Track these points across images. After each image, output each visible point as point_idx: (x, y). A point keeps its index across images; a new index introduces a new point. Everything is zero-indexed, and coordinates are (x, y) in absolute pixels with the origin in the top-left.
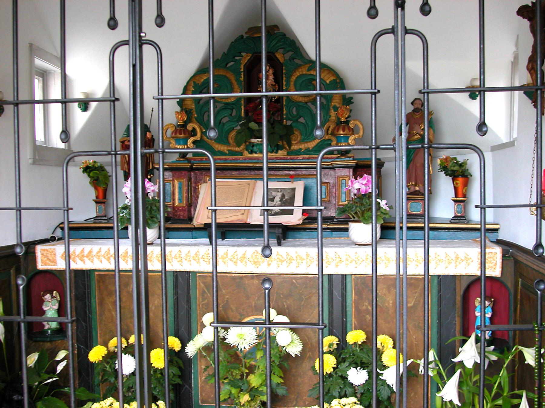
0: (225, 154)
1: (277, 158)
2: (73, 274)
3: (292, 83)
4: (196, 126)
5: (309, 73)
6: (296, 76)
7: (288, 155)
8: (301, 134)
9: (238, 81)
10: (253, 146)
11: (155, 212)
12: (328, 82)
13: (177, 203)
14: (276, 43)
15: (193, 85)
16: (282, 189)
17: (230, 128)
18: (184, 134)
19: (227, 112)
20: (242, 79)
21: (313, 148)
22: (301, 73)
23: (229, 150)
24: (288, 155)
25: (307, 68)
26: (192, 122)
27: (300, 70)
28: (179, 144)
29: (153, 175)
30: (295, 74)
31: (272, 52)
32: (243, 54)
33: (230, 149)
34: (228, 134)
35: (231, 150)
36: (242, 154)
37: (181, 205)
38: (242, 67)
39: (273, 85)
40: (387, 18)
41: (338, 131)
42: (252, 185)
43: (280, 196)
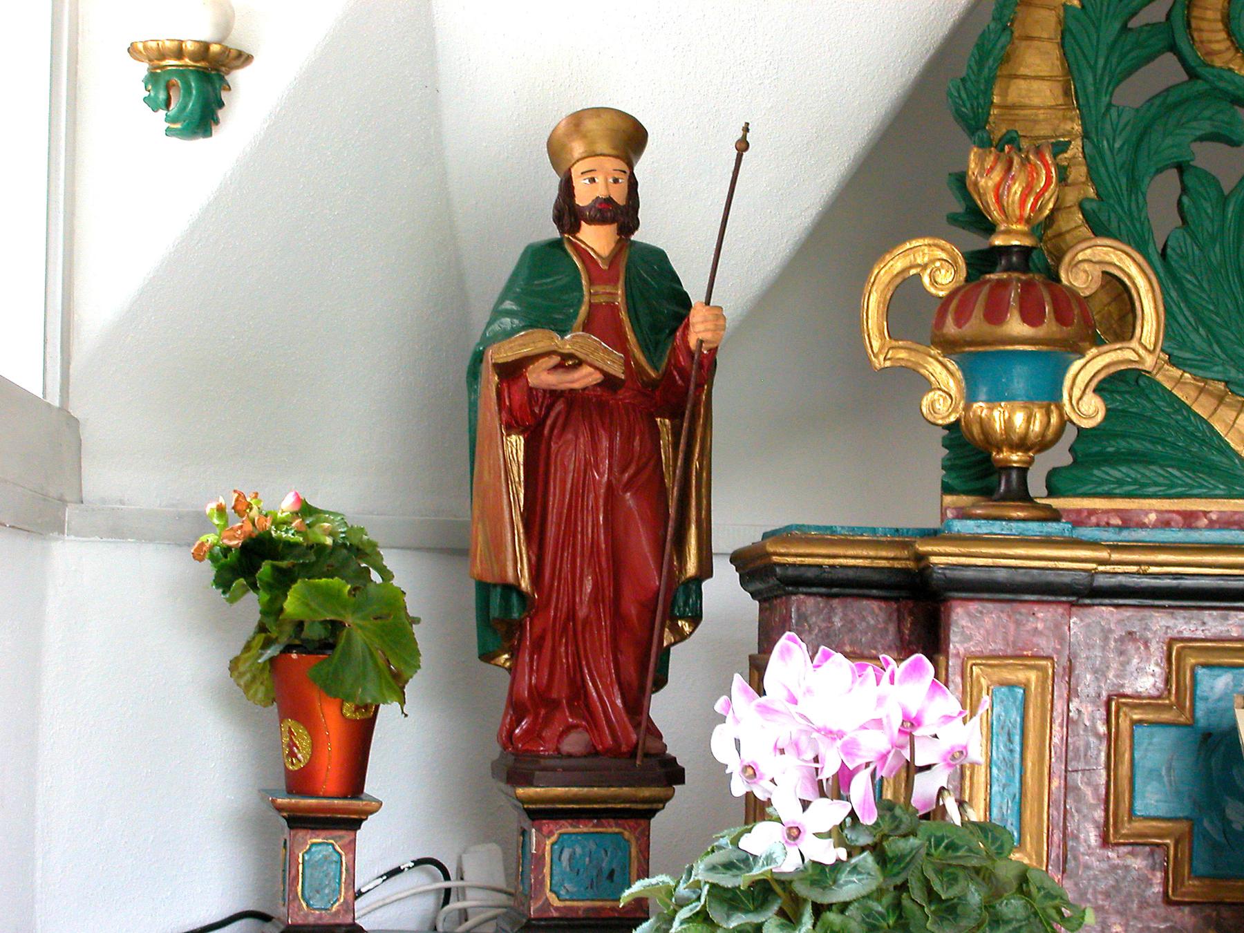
18: (1062, 318)
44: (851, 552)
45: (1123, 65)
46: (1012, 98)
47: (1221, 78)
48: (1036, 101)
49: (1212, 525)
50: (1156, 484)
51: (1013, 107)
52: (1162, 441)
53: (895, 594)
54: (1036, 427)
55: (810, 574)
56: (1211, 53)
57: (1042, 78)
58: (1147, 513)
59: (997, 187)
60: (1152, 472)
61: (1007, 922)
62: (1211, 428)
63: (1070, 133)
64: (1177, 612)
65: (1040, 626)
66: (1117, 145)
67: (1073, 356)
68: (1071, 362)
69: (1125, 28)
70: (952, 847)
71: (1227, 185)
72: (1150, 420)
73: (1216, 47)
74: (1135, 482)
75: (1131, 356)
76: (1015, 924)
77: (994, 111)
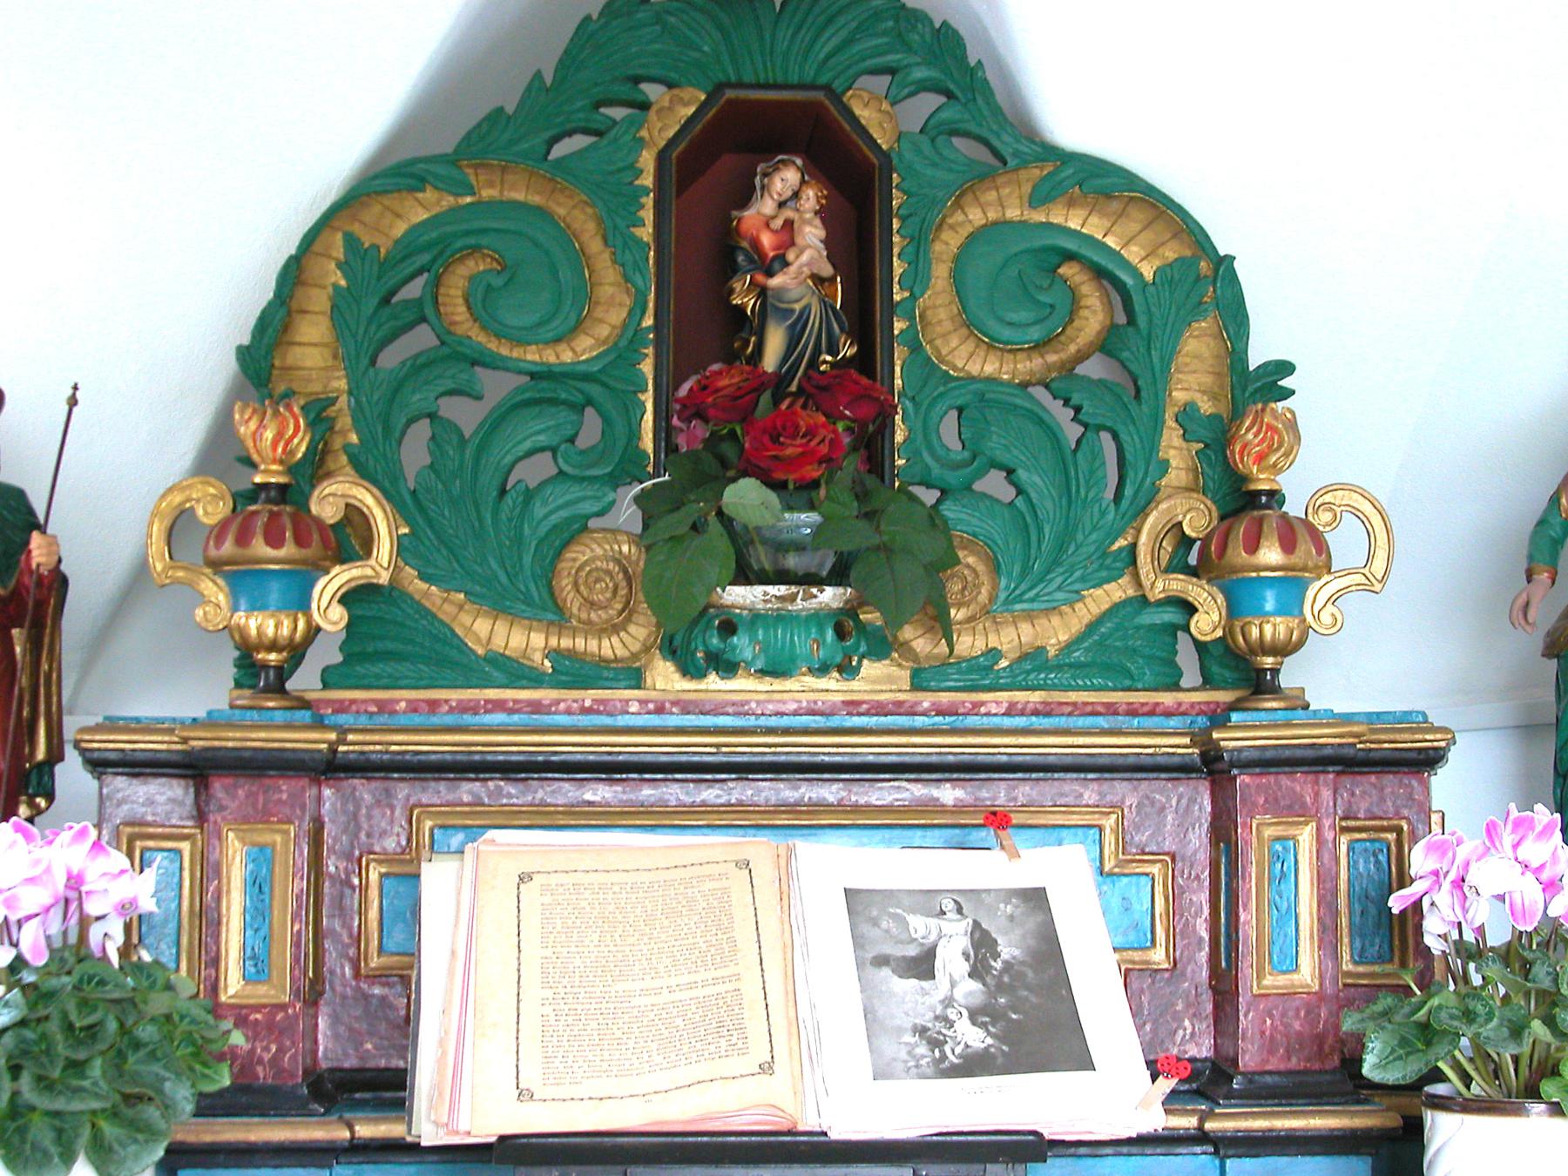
0: (534, 679)
1: (852, 706)
3: (941, 273)
4: (367, 498)
5: (1039, 217)
6: (965, 232)
7: (916, 687)
8: (995, 568)
9: (616, 237)
10: (729, 628)
11: (153, 1056)
12: (1148, 271)
13: (233, 985)
14: (849, 42)
15: (339, 252)
16: (964, 900)
17: (569, 521)
18: (300, 541)
19: (537, 429)
20: (646, 233)
21: (1069, 647)
22: (992, 215)
23: (554, 654)
24: (916, 687)
25: (1027, 189)
26: (329, 475)
27: (991, 196)
28: (256, 606)
29: (50, 798)
30: (959, 217)
31: (827, 88)
32: (652, 91)
33: (566, 643)
34: (558, 555)
35: (571, 654)
36: (635, 677)
37: (263, 993)
38: (647, 160)
39: (818, 280)
41: (1253, 546)
42: (765, 871)
43: (964, 942)
44: (148, 738)
45: (380, 334)
46: (290, 361)
47: (461, 344)
48: (309, 364)
49: (451, 710)
50: (407, 677)
51: (290, 368)
52: (411, 642)
53: (189, 772)
54: (285, 631)
55: (112, 756)
56: (455, 323)
57: (315, 345)
58: (398, 701)
59: (254, 434)
60: (403, 668)
61: (146, 1045)
62: (453, 631)
63: (338, 390)
64: (150, 780)
65: (284, 796)
66: (376, 397)
67: (315, 574)
68: (317, 579)
69: (386, 300)
70: (102, 983)
71: (467, 433)
72: (402, 625)
73: (458, 318)
74: (390, 676)
75: (369, 572)
76: (151, 1047)
77: (275, 372)
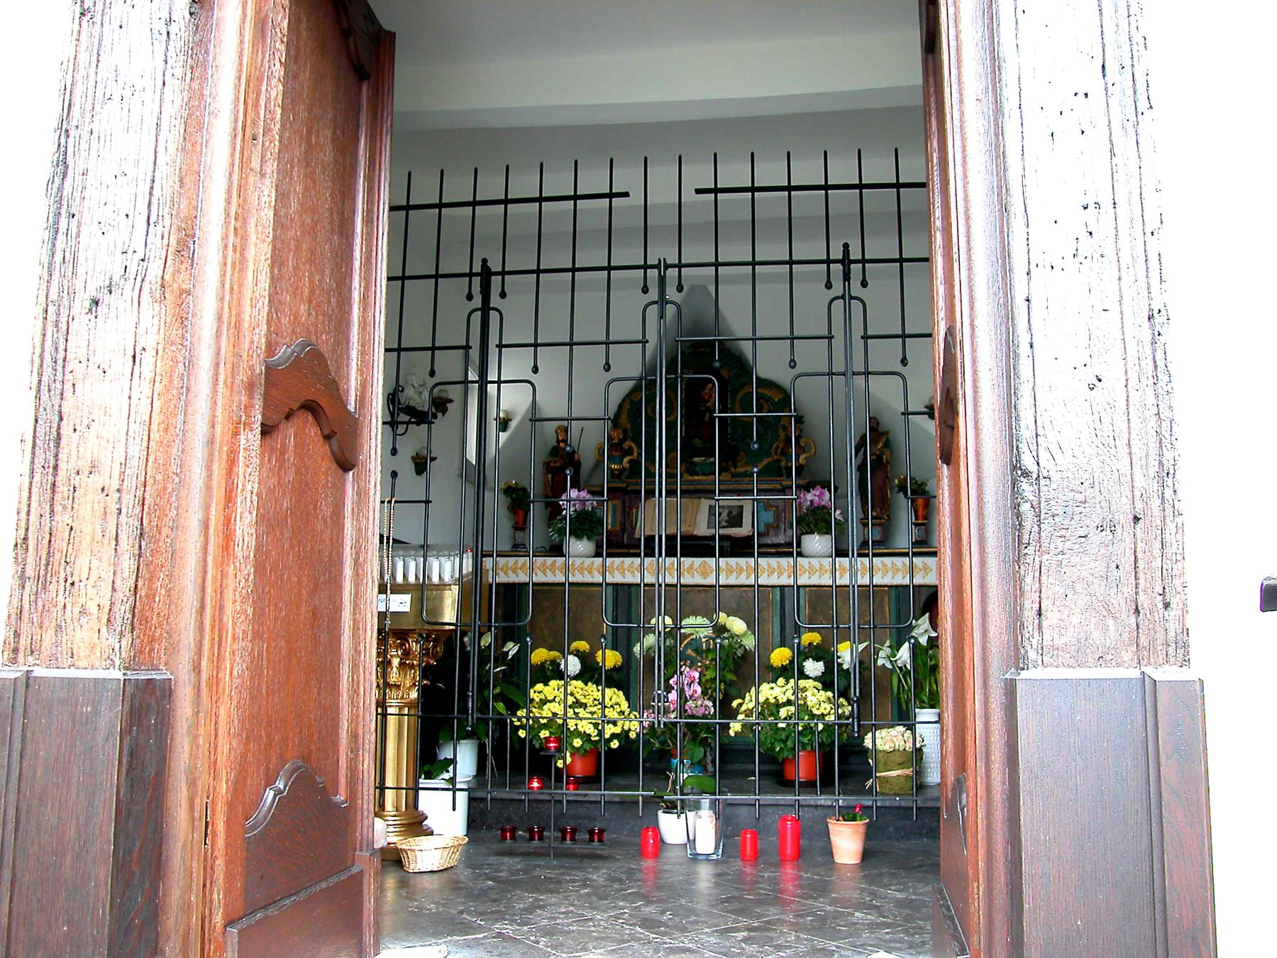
2: (502, 590)
40: (838, 288)
